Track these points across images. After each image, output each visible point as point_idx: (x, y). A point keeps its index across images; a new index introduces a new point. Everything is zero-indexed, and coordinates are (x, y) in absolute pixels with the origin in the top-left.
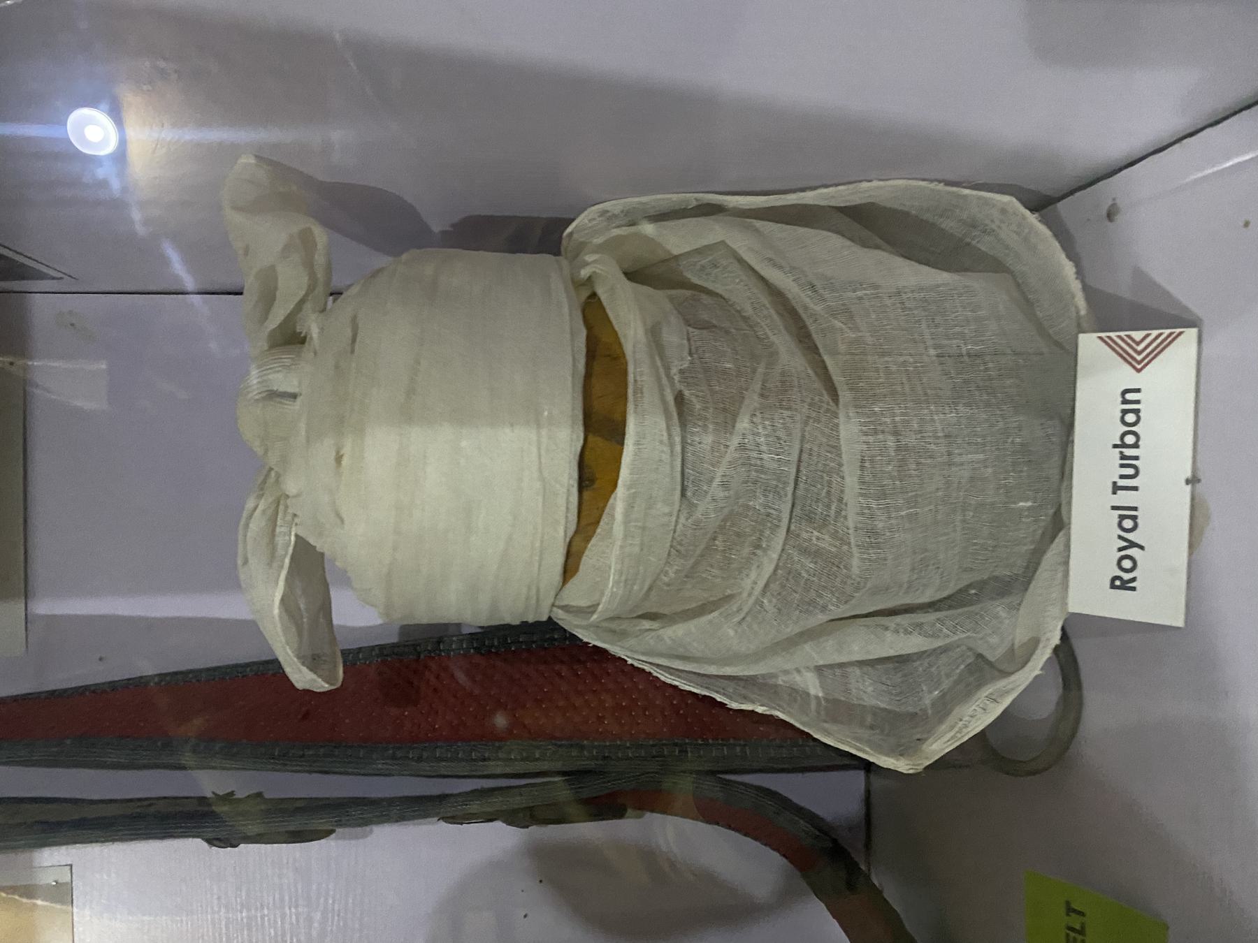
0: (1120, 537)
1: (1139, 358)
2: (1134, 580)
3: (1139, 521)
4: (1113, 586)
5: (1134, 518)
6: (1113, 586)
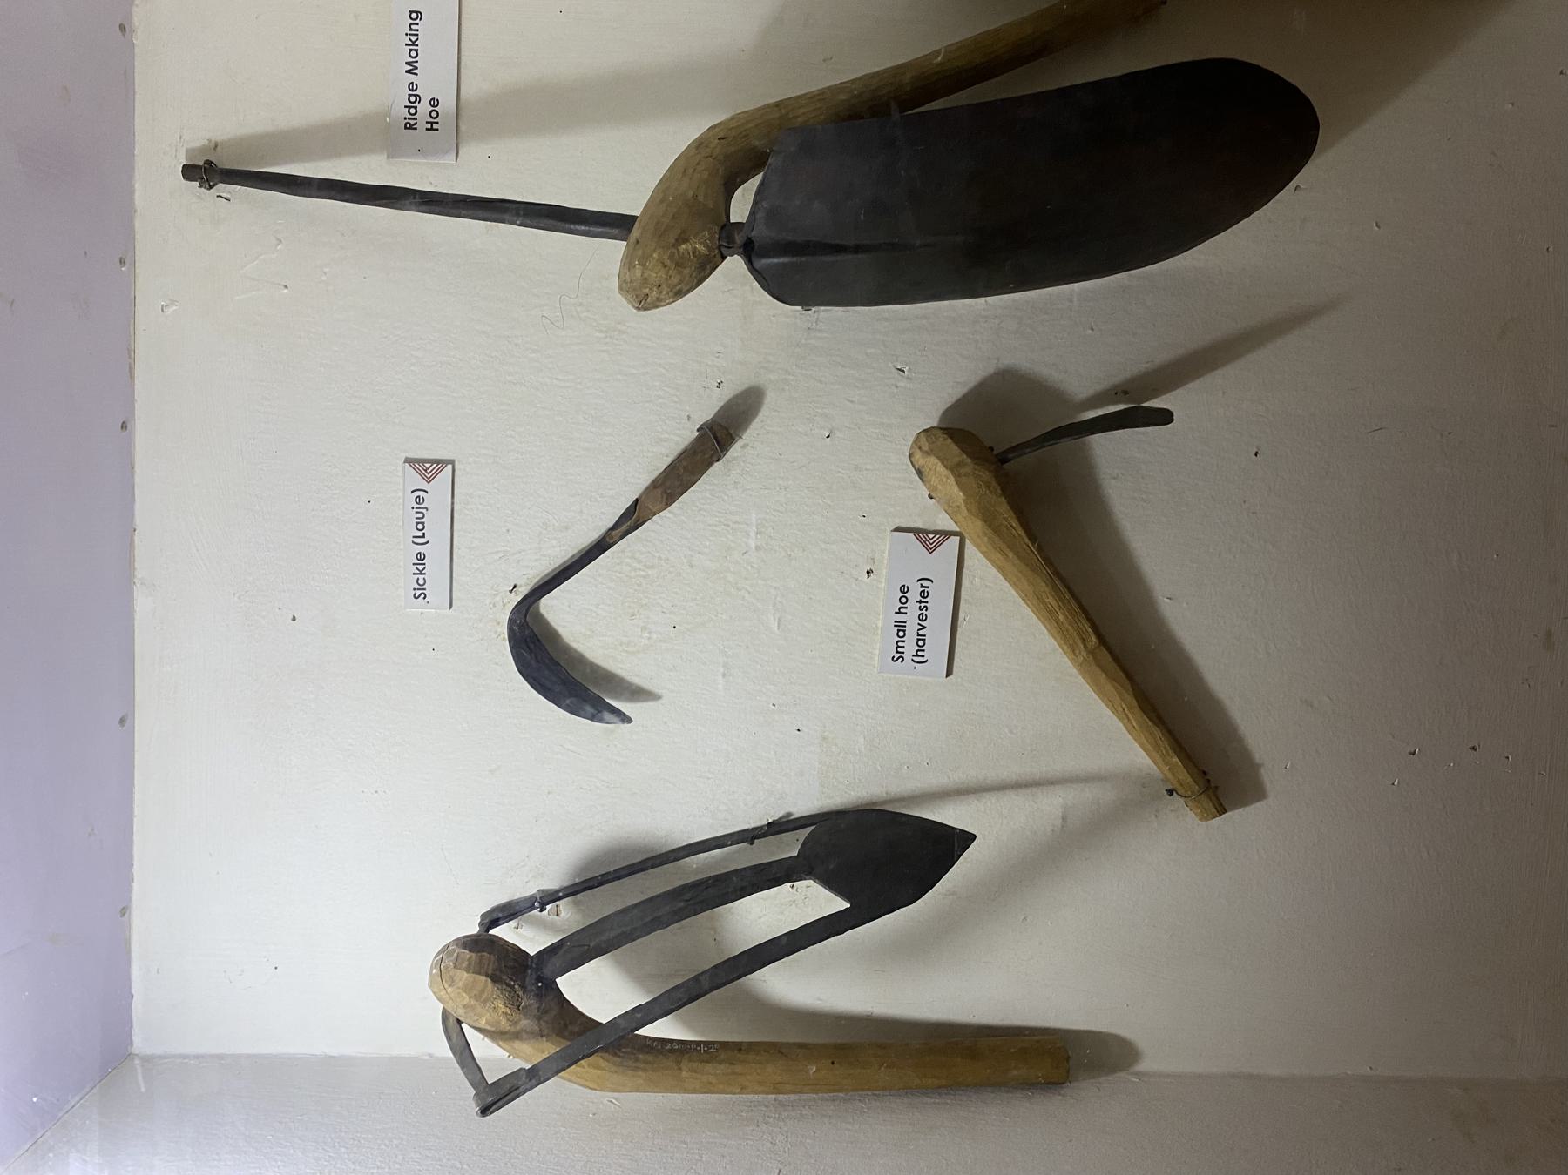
0: (919, 624)
1: (931, 546)
2: (416, 124)
4: (406, 128)
6: (406, 128)
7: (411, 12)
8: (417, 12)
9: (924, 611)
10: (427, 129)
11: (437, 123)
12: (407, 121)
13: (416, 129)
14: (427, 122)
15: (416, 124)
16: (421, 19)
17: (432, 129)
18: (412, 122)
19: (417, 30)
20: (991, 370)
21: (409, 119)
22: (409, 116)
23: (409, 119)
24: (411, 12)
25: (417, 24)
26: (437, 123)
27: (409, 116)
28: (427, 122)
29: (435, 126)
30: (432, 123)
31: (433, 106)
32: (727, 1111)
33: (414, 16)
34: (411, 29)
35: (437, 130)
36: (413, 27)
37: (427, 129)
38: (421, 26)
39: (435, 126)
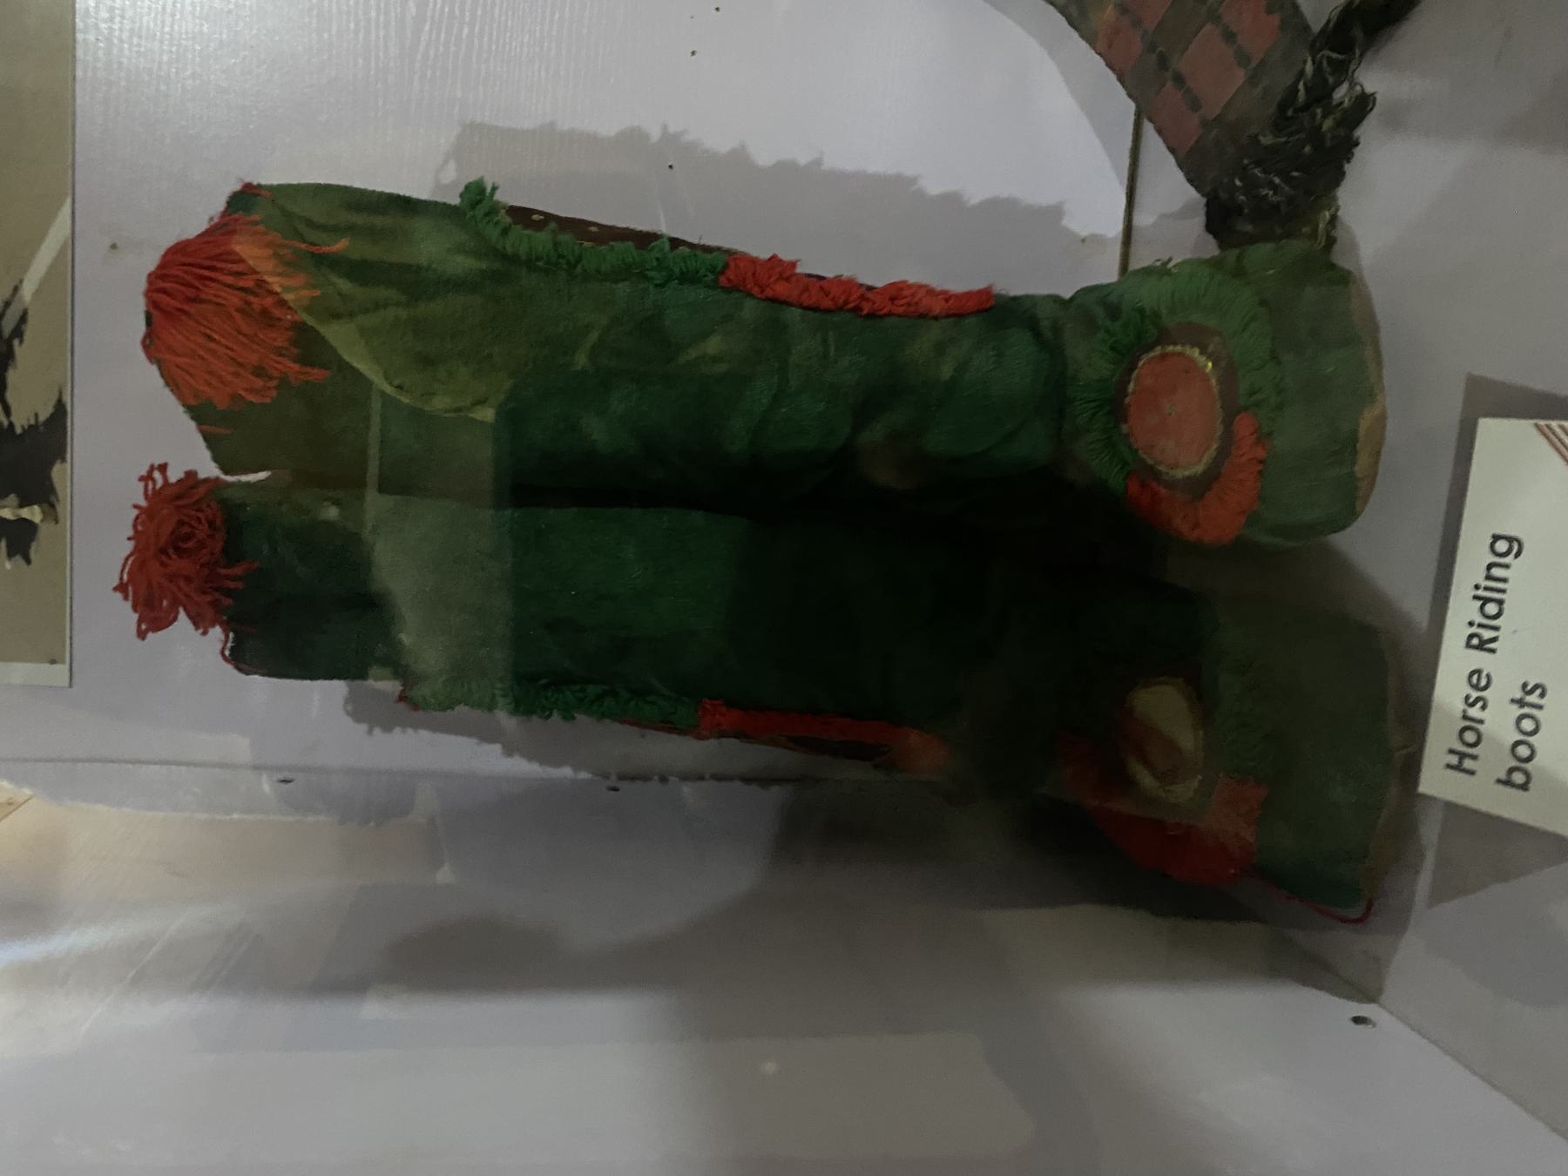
2: (1494, 640)
3: (1505, 606)
4: (1469, 645)
5: (1500, 602)
6: (1469, 645)
7: (1496, 538)
8: (1510, 539)
9: (1475, 694)
10: (1449, 766)
11: (1474, 757)
12: (1474, 630)
13: (1493, 651)
14: (1452, 751)
15: (1494, 640)
16: (1518, 555)
17: (1458, 768)
18: (1487, 634)
19: (1504, 580)
20: (892, 171)
21: (1481, 626)
22: (1479, 619)
23: (1481, 626)
24: (1496, 538)
25: (1507, 566)
26: (1474, 757)
27: (1479, 619)
28: (1452, 751)
29: (1468, 764)
30: (1462, 756)
31: (1476, 687)
32: (213, 77)
33: (1502, 546)
34: (1489, 577)
35: (1472, 773)
36: (1496, 572)
37: (1449, 766)
38: (1517, 572)
39: (1468, 764)
